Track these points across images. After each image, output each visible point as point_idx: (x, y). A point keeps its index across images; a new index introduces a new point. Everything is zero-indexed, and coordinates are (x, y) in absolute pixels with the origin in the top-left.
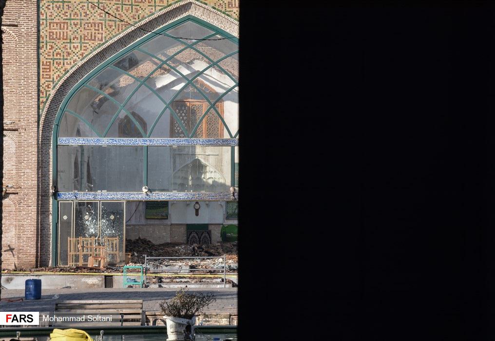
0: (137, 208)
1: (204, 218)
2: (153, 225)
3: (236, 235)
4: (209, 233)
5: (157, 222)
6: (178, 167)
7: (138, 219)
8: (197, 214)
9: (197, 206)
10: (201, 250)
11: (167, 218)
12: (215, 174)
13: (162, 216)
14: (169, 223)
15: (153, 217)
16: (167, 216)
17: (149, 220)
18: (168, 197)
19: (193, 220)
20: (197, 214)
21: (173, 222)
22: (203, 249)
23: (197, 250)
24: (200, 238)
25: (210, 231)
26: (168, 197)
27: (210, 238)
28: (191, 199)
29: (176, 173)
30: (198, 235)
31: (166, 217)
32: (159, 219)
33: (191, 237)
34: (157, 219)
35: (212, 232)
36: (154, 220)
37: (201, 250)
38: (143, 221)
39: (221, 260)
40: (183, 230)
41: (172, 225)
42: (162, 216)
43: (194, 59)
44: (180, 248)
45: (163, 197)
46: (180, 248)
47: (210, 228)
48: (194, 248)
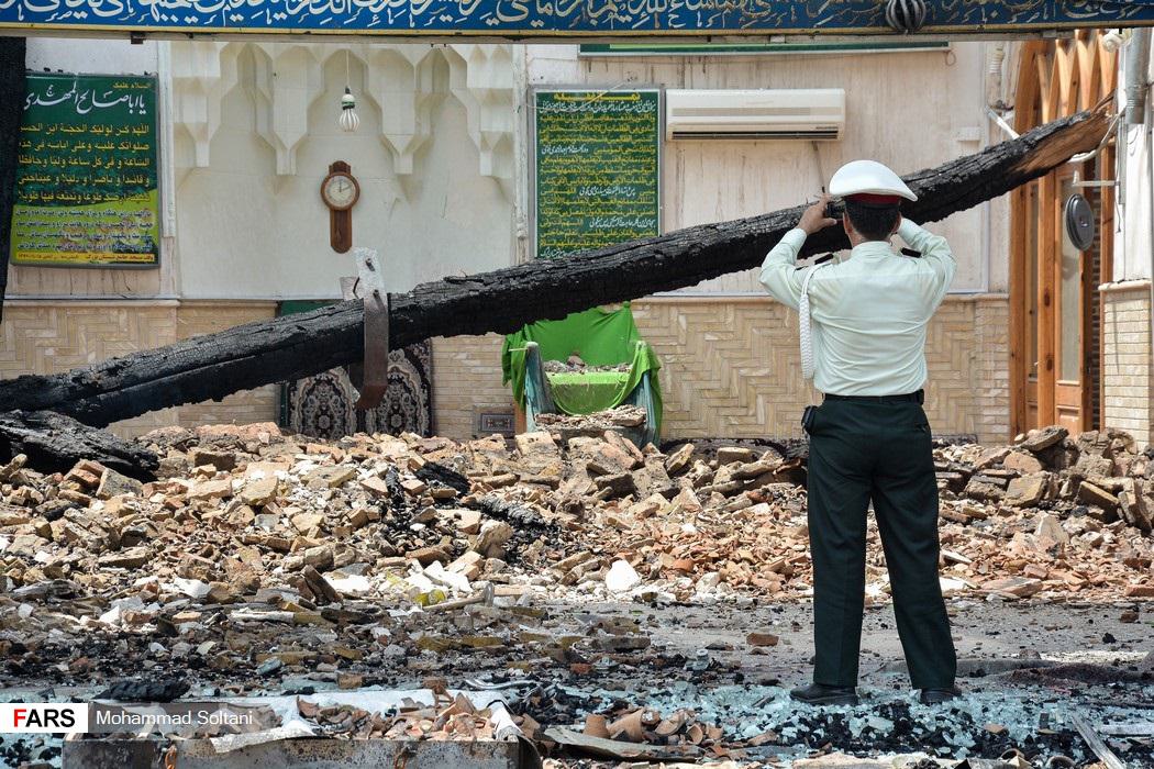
8: (341, 240)
9: (340, 194)
11: (156, 264)
16: (155, 251)
20: (341, 240)
27: (427, 385)
31: (150, 256)
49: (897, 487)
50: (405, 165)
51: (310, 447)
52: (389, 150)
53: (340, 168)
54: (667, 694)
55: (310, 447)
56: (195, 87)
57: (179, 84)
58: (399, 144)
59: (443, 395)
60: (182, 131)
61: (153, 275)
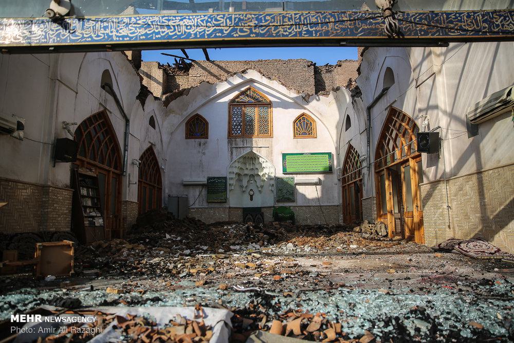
0: (200, 194)
1: (257, 202)
2: (214, 208)
3: (374, 195)
4: (262, 214)
5: (216, 205)
6: (235, 158)
7: (201, 203)
8: (251, 199)
9: (252, 193)
10: (259, 230)
11: (226, 202)
12: (267, 163)
13: (221, 200)
14: (228, 206)
15: (213, 201)
16: (226, 200)
17: (210, 204)
18: (143, 31)
19: (248, 204)
20: (251, 199)
21: (231, 206)
22: (261, 229)
23: (252, 231)
24: (254, 219)
25: (263, 213)
26: (143, 31)
27: (263, 219)
28: (229, 35)
29: (233, 163)
30: (252, 216)
31: (225, 201)
32: (219, 203)
33: (247, 218)
34: (217, 202)
35: (265, 214)
36: (214, 204)
37: (259, 230)
38: (205, 205)
39: (290, 245)
40: (240, 212)
41: (230, 208)
42: (221, 200)
43: (247, 69)
44: (229, 227)
45: (124, 31)
46: (229, 227)
47: (263, 210)
48: (248, 228)
49: (57, 116)
50: (260, 189)
51: (82, 294)
52: (258, 187)
53: (251, 190)
54: (309, 300)
55: (82, 294)
56: (232, 179)
57: (230, 178)
58: (259, 186)
59: (265, 220)
60: (230, 185)
61: (225, 204)
